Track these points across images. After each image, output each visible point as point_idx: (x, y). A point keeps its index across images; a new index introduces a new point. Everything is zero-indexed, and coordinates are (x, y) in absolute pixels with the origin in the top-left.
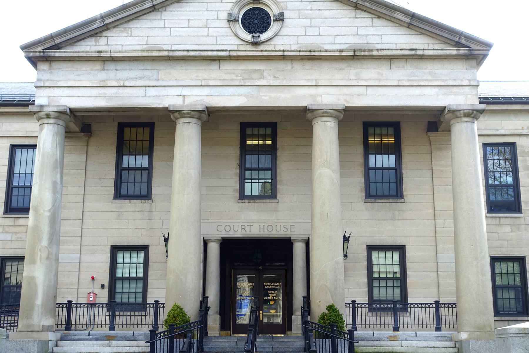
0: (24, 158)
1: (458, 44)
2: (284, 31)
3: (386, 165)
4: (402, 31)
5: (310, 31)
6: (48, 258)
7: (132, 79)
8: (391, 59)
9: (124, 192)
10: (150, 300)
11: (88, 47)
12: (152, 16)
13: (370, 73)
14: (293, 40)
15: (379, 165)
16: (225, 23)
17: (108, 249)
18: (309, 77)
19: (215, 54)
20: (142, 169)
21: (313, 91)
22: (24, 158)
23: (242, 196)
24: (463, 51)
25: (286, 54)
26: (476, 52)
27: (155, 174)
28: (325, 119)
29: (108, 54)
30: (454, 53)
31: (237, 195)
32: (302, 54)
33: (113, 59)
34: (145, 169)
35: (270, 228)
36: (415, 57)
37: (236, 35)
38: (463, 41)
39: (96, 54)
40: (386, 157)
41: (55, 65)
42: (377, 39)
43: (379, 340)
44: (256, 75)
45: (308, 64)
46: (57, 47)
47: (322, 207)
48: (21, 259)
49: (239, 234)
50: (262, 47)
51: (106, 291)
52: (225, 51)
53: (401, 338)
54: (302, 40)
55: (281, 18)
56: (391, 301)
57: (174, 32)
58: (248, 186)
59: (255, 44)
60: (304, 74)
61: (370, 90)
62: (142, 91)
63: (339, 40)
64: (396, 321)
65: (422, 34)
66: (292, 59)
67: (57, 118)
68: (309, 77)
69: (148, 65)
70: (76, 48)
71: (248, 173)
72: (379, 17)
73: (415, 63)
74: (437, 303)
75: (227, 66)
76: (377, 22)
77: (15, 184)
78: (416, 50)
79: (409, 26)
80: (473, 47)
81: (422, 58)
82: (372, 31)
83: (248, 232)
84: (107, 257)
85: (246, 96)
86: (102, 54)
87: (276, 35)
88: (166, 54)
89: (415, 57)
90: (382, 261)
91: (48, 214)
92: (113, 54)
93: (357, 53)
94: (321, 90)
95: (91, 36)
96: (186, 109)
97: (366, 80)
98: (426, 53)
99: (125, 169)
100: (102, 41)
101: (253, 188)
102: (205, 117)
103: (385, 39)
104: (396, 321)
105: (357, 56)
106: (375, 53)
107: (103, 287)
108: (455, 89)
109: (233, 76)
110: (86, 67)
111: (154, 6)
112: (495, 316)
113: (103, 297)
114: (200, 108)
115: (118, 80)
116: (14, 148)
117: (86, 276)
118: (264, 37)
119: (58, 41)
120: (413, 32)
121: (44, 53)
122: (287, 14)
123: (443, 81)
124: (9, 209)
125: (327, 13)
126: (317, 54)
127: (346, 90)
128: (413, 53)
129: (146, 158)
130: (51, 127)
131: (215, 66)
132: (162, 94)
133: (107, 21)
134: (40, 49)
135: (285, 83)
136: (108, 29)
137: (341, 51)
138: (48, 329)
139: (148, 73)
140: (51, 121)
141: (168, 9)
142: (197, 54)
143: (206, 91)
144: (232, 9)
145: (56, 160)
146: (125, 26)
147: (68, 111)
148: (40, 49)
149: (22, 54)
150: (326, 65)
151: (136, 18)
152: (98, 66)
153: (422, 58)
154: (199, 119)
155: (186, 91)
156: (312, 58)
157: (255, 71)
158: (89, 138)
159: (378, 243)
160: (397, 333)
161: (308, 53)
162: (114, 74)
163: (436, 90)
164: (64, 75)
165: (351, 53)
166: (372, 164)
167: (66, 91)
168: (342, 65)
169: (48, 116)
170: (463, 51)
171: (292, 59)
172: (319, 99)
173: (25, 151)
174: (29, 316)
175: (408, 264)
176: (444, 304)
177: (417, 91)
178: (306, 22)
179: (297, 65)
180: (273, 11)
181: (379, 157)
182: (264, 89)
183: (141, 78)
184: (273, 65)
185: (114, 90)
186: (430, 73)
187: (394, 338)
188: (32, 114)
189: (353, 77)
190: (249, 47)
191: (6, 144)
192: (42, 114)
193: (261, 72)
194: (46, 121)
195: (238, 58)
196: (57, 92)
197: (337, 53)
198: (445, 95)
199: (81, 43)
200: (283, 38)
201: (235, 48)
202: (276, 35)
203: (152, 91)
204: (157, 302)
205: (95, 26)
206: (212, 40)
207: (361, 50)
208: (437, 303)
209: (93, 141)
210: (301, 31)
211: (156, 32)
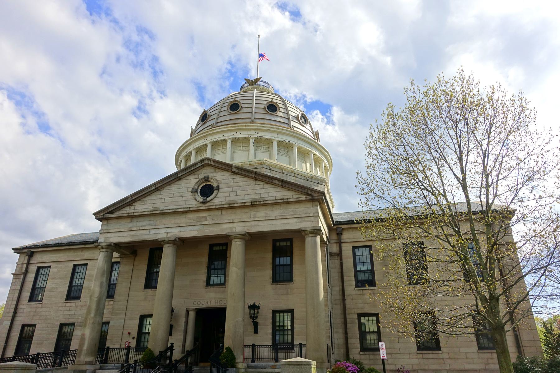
0: (79, 271)
1: (308, 194)
2: (219, 195)
3: (285, 263)
4: (280, 189)
5: (232, 194)
6: (93, 323)
7: (144, 226)
8: (272, 205)
9: (278, 279)
10: (296, 343)
11: (125, 211)
12: (156, 193)
13: (261, 213)
14: (223, 199)
15: (281, 263)
16: (190, 194)
17: (138, 317)
18: (230, 218)
19: (182, 210)
20: (287, 265)
21: (231, 225)
22: (79, 271)
23: (208, 284)
24: (309, 197)
25: (217, 207)
26: (316, 198)
27: (295, 267)
28: (236, 240)
29: (132, 214)
30: (304, 199)
31: (205, 284)
32: (225, 206)
33: (136, 216)
34: (289, 265)
35: (221, 302)
36: (283, 203)
37: (195, 199)
38: (309, 192)
39: (127, 215)
40: (285, 258)
41: (110, 221)
42: (266, 195)
43: (265, 368)
44: (203, 219)
45: (230, 211)
46: (111, 212)
47: (241, 289)
48: (73, 324)
49: (204, 306)
50: (207, 204)
51: (135, 340)
52: (187, 208)
53: (278, 367)
54: (228, 199)
55: (218, 188)
56: (282, 345)
57: (166, 200)
58: (212, 278)
59: (204, 203)
60: (227, 216)
61: (261, 223)
62: (147, 232)
63: (246, 197)
64: (277, 356)
65: (289, 190)
66: (222, 209)
67: (107, 248)
68: (230, 218)
69: (152, 218)
70: (120, 212)
71: (212, 271)
72: (267, 183)
73: (285, 206)
74: (254, 345)
75: (190, 216)
76: (266, 186)
77: (112, 283)
78: (283, 199)
79: (282, 186)
80: (314, 195)
81: (288, 203)
82: (263, 191)
83: (209, 305)
84: (137, 322)
85: (197, 230)
86: (130, 215)
87: (215, 197)
88: (159, 212)
89: (283, 203)
90: (281, 319)
91: (96, 299)
92: (135, 214)
93: (253, 204)
94: (235, 224)
95: (128, 206)
96: (166, 240)
97: (258, 217)
98: (289, 200)
99: (278, 265)
100: (133, 208)
101: (214, 279)
102: (247, 238)
103: (270, 195)
104: (277, 356)
105: (254, 205)
106: (262, 203)
107: (134, 338)
108: (306, 219)
109: (192, 221)
110: (124, 221)
111: (156, 188)
112: (418, 350)
113: (133, 344)
114: (173, 239)
115: (229, 220)
116: (75, 266)
117: (126, 332)
118: (209, 199)
119: (110, 210)
120: (285, 190)
121: (103, 216)
122: (221, 186)
123: (300, 214)
124: (69, 297)
125: (241, 184)
126: (232, 205)
127: (248, 224)
128: (282, 201)
129: (289, 258)
130: (103, 253)
131: (184, 216)
132: (157, 232)
133: (134, 198)
134: (102, 214)
135: (217, 222)
136: (136, 202)
137: (245, 203)
138: (90, 363)
139: (152, 222)
140: (104, 250)
141: (165, 189)
142: (173, 211)
143: (178, 230)
144: (194, 186)
145: (104, 270)
146: (144, 199)
147: (177, 240)
148: (102, 214)
149: (94, 217)
150: (239, 211)
151: (149, 195)
152: (129, 220)
153: (288, 203)
154: (174, 244)
155: (169, 230)
156: (230, 207)
157: (203, 217)
158: (135, 256)
159: (278, 309)
160: (277, 363)
161: (228, 206)
162: (141, 223)
163: (296, 220)
164: (114, 226)
165: (250, 204)
166: (278, 263)
167: (113, 234)
168: (246, 210)
169: (102, 248)
170: (309, 197)
171: (222, 209)
172: (234, 229)
173: (360, 249)
174: (79, 357)
175: (295, 320)
176: (258, 346)
177: (285, 221)
178: (230, 189)
179: (224, 212)
180: (215, 185)
181: (281, 259)
182: (206, 226)
183: (148, 225)
184: (212, 213)
185: (135, 232)
186: (293, 211)
187: (274, 367)
188: (96, 247)
189: (252, 216)
190: (201, 205)
191: (71, 265)
192: (100, 247)
193: (205, 218)
194: (102, 250)
195: (194, 211)
196: (109, 235)
197: (243, 204)
198: (301, 222)
199: (123, 209)
200: (218, 199)
201: (194, 206)
202: (215, 197)
203: (153, 232)
204: (300, 344)
205: (128, 201)
206: (183, 203)
207: (255, 202)
208: (254, 345)
209: (137, 258)
210: (227, 194)
211: (158, 201)
